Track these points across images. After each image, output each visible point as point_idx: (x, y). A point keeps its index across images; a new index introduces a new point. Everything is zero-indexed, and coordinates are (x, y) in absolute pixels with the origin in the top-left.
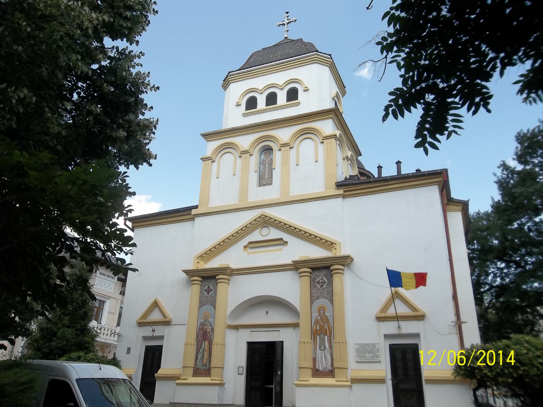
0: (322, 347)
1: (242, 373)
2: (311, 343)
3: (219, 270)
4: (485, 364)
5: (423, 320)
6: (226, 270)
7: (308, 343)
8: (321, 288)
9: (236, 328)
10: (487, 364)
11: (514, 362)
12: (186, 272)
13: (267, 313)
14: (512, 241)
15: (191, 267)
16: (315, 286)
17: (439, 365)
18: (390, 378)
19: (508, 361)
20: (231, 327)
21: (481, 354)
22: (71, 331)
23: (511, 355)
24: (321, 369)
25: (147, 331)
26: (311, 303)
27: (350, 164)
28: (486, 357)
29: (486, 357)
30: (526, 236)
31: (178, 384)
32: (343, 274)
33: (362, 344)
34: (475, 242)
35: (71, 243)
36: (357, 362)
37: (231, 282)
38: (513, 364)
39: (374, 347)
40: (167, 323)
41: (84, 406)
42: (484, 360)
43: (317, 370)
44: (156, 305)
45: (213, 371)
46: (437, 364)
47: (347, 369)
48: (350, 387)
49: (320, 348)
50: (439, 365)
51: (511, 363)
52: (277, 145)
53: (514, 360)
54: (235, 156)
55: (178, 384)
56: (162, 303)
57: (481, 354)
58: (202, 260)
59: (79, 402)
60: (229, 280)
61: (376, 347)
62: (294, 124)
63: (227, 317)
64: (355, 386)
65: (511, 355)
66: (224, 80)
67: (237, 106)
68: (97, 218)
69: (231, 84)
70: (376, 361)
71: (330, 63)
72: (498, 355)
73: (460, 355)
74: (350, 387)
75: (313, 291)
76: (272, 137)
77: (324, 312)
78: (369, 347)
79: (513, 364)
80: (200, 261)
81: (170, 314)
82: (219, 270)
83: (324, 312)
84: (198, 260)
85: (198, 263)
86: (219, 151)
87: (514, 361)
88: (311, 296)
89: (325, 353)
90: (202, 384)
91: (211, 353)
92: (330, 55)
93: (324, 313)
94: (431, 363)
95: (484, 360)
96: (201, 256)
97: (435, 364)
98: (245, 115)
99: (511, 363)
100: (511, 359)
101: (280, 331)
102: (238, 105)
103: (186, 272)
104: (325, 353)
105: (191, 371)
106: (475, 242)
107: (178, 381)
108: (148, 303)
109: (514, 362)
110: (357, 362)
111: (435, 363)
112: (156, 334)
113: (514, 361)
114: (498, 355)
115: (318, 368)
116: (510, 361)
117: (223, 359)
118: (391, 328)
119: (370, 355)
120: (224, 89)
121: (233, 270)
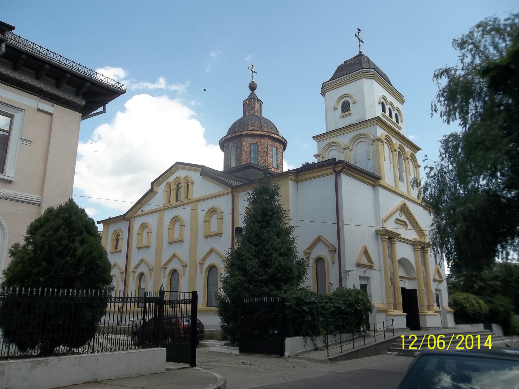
11: (491, 346)
14: (250, 289)
19: (485, 345)
21: (460, 337)
23: (489, 339)
27: (386, 143)
28: (464, 341)
29: (464, 341)
30: (150, 321)
38: (490, 348)
42: (463, 345)
51: (489, 347)
53: (491, 344)
54: (338, 151)
57: (460, 337)
62: (385, 129)
65: (489, 339)
66: (321, 89)
67: (335, 110)
69: (326, 93)
72: (475, 340)
76: (361, 134)
79: (490, 348)
86: (327, 149)
91: (176, 369)
95: (463, 345)
98: (342, 117)
99: (489, 347)
102: (335, 109)
109: (491, 346)
111: (416, 347)
114: (475, 340)
120: (323, 96)
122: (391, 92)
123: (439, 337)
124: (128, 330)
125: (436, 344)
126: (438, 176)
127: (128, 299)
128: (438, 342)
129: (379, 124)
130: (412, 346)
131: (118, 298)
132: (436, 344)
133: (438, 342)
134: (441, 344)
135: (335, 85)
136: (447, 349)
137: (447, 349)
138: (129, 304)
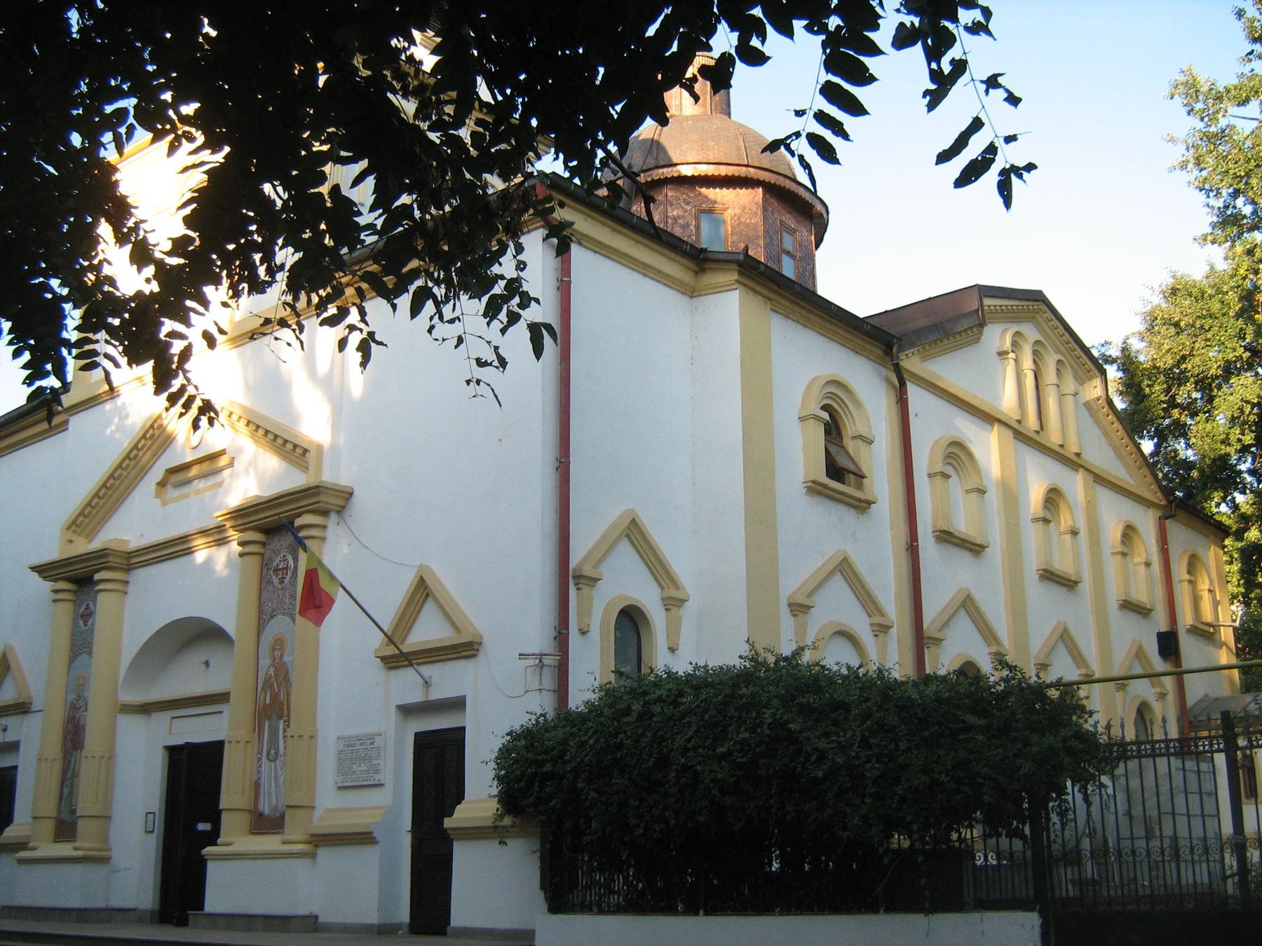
0: (273, 751)
1: (151, 829)
2: (248, 742)
3: (82, 561)
5: (474, 656)
6: (106, 555)
7: (238, 742)
8: (280, 586)
9: (146, 709)
12: (43, 570)
13: (207, 664)
15: (52, 552)
16: (270, 582)
18: (409, 827)
20: (127, 709)
22: (1236, 590)
24: (267, 811)
25: (407, 688)
26: (259, 632)
31: (21, 861)
32: (323, 539)
33: (350, 737)
36: (340, 788)
37: (130, 589)
39: (372, 743)
40: (466, 650)
43: (261, 815)
44: (422, 591)
45: (82, 825)
47: (314, 807)
48: (313, 856)
49: (268, 754)
55: (21, 861)
56: (447, 578)
58: (79, 535)
60: (127, 583)
61: (376, 745)
63: (120, 682)
64: (323, 853)
70: (372, 783)
74: (313, 856)
75: (265, 594)
77: (282, 655)
78: (361, 744)
80: (74, 537)
81: (480, 620)
82: (82, 561)
83: (282, 655)
84: (70, 536)
85: (71, 541)
88: (261, 611)
89: (275, 766)
90: (37, 860)
93: (281, 658)
96: (74, 523)
101: (221, 712)
103: (43, 570)
104: (275, 766)
105: (48, 827)
107: (23, 854)
108: (403, 585)
110: (340, 788)
112: (439, 693)
115: (262, 810)
117: (107, 798)
118: (407, 688)
119: (364, 768)
121: (129, 553)
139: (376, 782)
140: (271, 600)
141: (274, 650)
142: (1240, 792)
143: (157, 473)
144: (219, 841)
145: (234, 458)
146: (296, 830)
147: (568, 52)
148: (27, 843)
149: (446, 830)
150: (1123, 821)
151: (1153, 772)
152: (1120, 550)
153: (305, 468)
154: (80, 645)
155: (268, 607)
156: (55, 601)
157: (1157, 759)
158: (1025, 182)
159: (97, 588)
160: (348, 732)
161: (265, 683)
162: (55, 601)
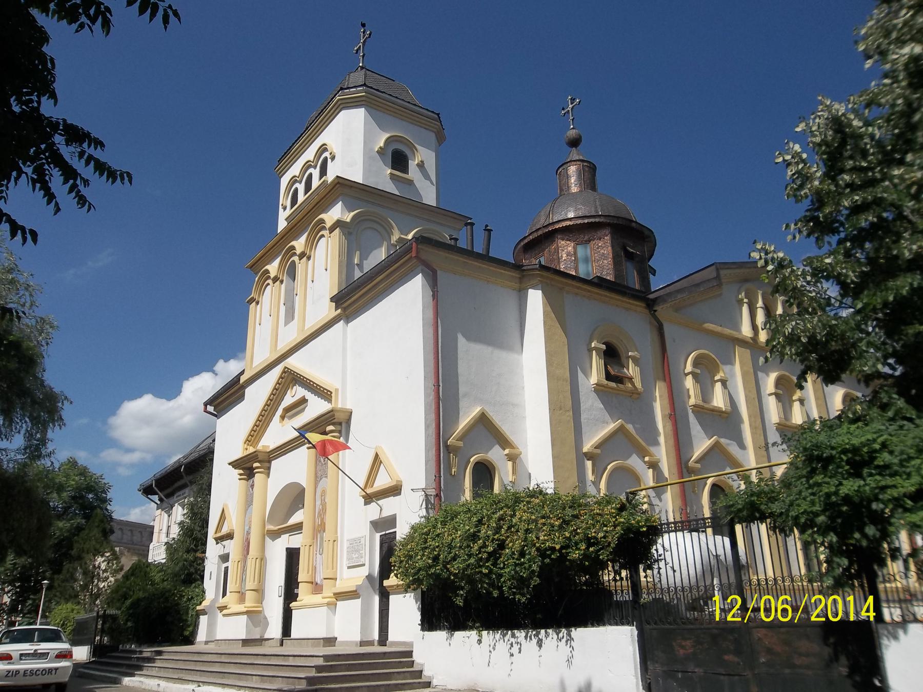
2: (311, 546)
4: (824, 619)
10: (827, 618)
16: (320, 461)
17: (745, 621)
23: (869, 604)
25: (373, 512)
29: (826, 606)
34: (820, 98)
35: (684, 611)
39: (360, 542)
41: (1, 681)
46: (743, 619)
50: (745, 621)
52: (379, 232)
59: (175, 658)
65: (869, 604)
68: (769, 651)
71: (437, 127)
72: (845, 604)
73: (783, 603)
75: (318, 468)
87: (875, 614)
88: (316, 477)
92: (438, 114)
94: (733, 616)
96: (247, 440)
97: (740, 619)
100: (868, 611)
106: (820, 98)
107: (225, 612)
113: (875, 614)
114: (845, 604)
116: (868, 614)
118: (373, 512)
119: (357, 556)
122: (328, 119)
123: (781, 599)
124: (783, 575)
125: (776, 610)
126: (134, 550)
127: (692, 523)
128: (780, 608)
129: (220, 400)
130: (733, 616)
131: (673, 523)
132: (776, 610)
133: (780, 608)
134: (784, 611)
135: (297, 154)
136: (796, 621)
137: (796, 621)
138: (666, 536)
139: (362, 563)
140: (320, 471)
141: (322, 496)
142: (333, 676)
143: (280, 412)
144: (298, 599)
145: (71, 403)
146: (328, 591)
147: (37, 62)
148: (226, 606)
149: (385, 587)
150: (670, 572)
151: (243, 653)
152: (773, 391)
153: (330, 401)
154: (248, 502)
155: (319, 475)
156: (240, 479)
157: (671, 534)
158: (166, 28)
159: (255, 471)
160: (353, 537)
161: (319, 513)
162: (240, 479)
